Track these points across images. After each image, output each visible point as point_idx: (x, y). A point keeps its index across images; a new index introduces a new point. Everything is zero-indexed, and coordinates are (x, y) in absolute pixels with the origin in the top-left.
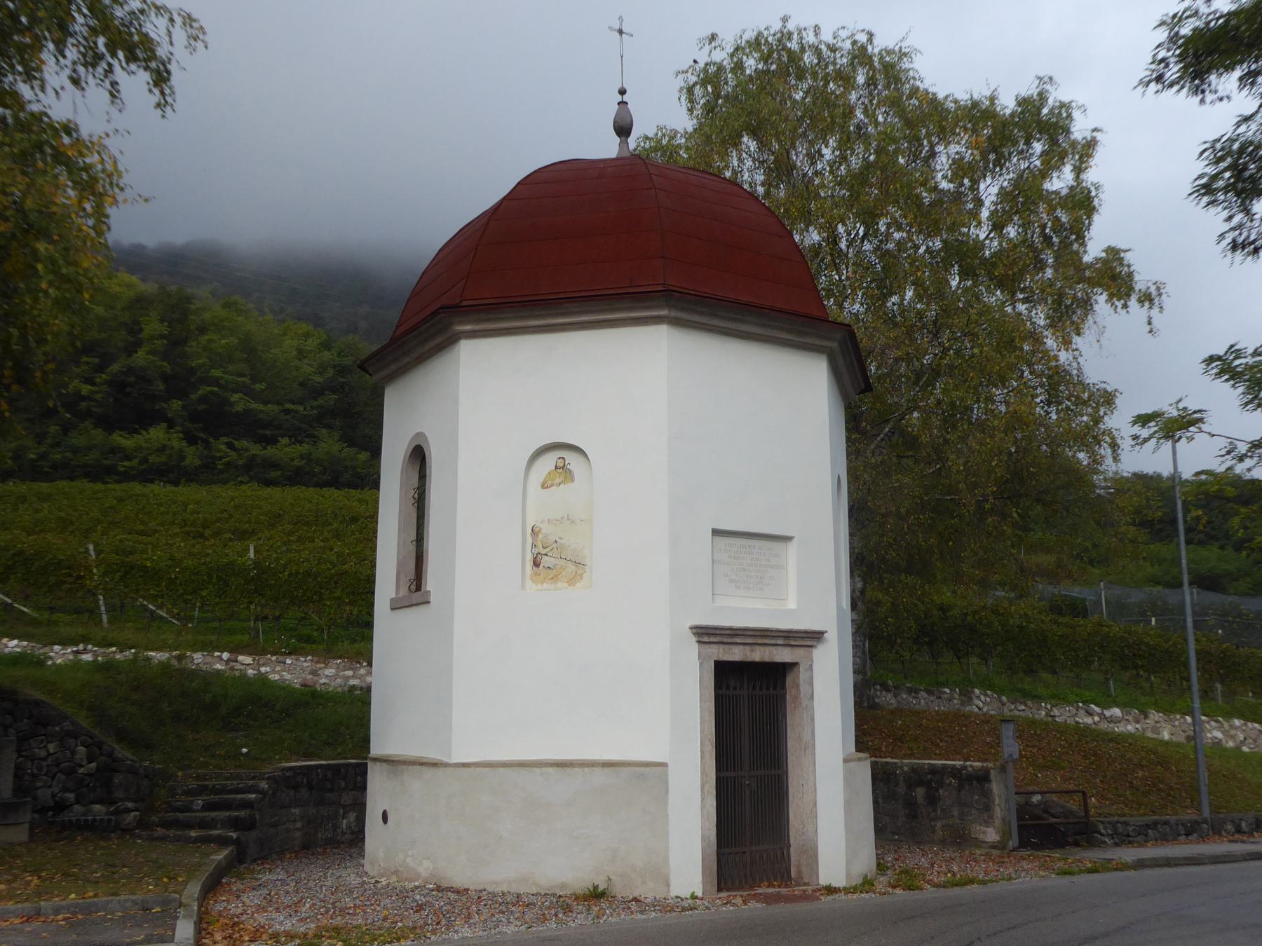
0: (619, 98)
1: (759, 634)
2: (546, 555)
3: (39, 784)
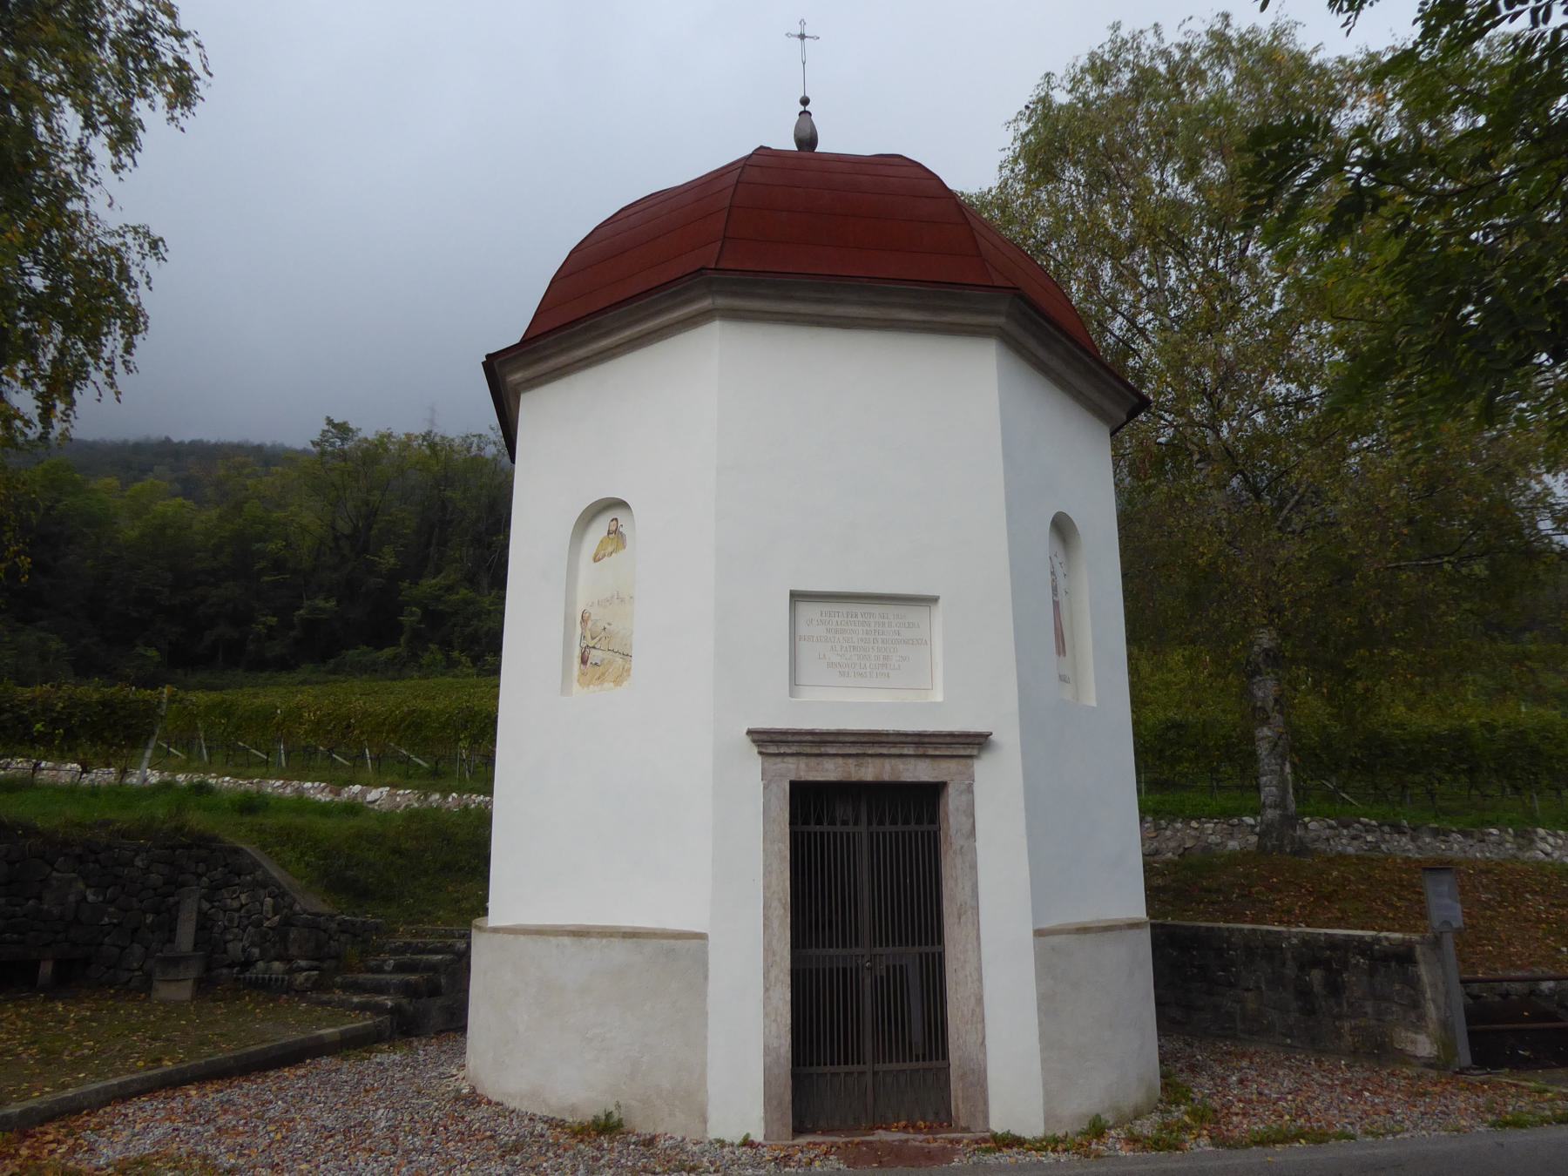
0: (802, 108)
1: (865, 739)
2: (594, 647)
3: (230, 937)
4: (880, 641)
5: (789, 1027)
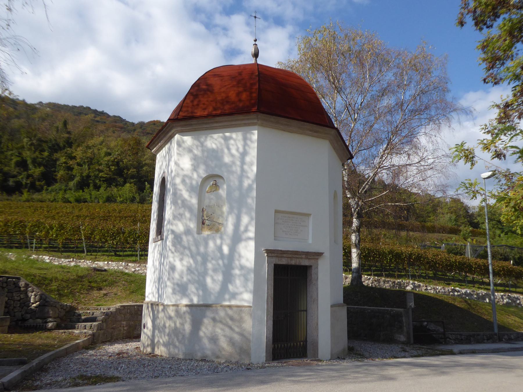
0: (254, 43)
5: (272, 332)
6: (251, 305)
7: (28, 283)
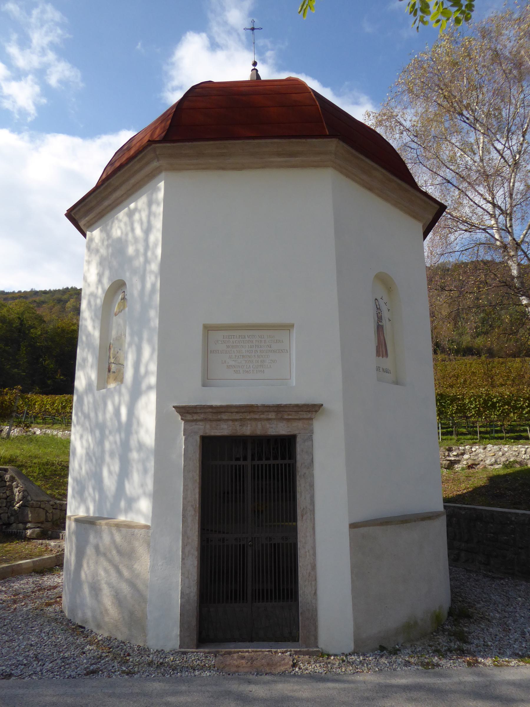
0: (253, 68)
4: (259, 351)
6: (149, 524)
7: (14, 475)
